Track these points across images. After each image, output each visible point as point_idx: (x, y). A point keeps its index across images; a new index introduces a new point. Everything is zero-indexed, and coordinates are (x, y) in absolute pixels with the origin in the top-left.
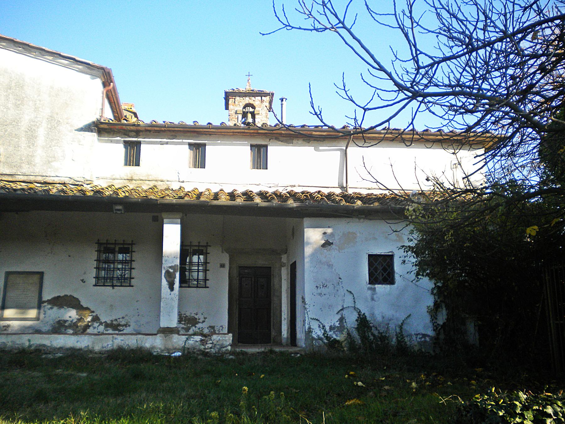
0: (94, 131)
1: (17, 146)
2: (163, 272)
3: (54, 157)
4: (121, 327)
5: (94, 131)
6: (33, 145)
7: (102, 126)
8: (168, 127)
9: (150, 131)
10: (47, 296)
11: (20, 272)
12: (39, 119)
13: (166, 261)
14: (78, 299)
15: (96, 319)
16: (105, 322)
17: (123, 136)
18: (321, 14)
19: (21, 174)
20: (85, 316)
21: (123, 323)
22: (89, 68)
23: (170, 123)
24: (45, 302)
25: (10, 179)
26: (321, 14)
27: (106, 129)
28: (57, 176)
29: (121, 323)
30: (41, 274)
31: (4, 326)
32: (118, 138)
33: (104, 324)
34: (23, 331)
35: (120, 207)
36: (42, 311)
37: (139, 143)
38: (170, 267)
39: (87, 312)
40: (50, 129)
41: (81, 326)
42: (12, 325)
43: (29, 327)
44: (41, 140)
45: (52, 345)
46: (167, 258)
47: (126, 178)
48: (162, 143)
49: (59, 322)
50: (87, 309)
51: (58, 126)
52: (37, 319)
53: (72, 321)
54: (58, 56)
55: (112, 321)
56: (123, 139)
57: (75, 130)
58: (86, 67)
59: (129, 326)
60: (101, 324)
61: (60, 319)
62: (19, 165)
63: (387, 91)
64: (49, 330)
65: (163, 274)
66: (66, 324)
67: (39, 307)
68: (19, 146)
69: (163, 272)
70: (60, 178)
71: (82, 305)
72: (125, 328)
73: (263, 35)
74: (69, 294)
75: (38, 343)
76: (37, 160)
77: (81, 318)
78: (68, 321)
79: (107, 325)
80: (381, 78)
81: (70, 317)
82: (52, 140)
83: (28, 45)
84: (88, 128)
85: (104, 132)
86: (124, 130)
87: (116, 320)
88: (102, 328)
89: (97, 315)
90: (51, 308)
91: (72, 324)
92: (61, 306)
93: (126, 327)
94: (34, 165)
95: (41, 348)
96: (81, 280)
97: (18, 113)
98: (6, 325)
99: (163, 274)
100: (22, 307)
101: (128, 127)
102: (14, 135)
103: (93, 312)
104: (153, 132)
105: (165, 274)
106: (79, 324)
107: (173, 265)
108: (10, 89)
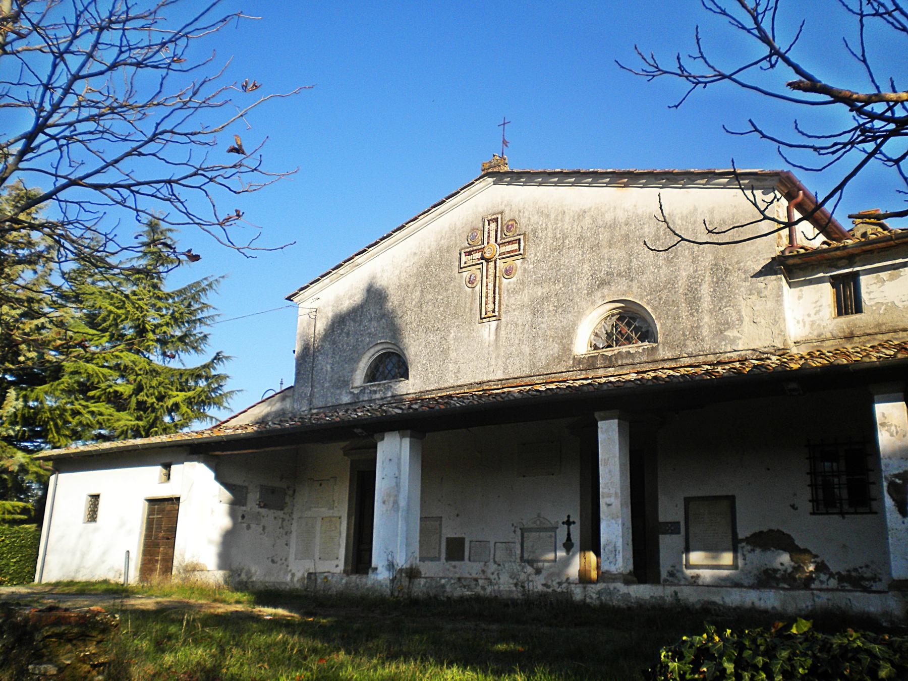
0: (779, 272)
1: (676, 317)
2: (885, 484)
3: (728, 323)
4: (867, 583)
5: (779, 272)
6: (697, 310)
7: (791, 261)
8: (897, 239)
9: (871, 251)
10: (743, 533)
11: (706, 497)
12: (700, 272)
13: (887, 466)
14: (789, 536)
15: (821, 567)
16: (838, 573)
17: (828, 270)
18: (695, 58)
19: (686, 355)
20: (805, 564)
21: (868, 574)
22: (757, 180)
23: (902, 230)
24: (742, 541)
25: (673, 365)
26: (695, 58)
27: (799, 265)
28: (735, 351)
29: (865, 576)
30: (731, 499)
31: (692, 577)
32: (821, 275)
33: (836, 577)
34: (719, 584)
35: (793, 385)
36: (739, 555)
37: (856, 275)
38: (897, 476)
39: (806, 557)
40: (717, 283)
41: (800, 578)
42: (702, 575)
43: (726, 579)
44: (706, 303)
45: (724, 602)
46: (887, 461)
47: (841, 335)
48: (895, 266)
49: (766, 572)
50: (806, 551)
51: (726, 277)
52: (735, 566)
53: (785, 571)
54: (712, 175)
55: (848, 571)
56: (828, 275)
57: (752, 277)
58: (755, 179)
59: (880, 580)
60: (831, 575)
61: (768, 567)
62: (682, 343)
63: (219, 241)
64: (753, 584)
65: (885, 489)
66: (778, 576)
67: (735, 550)
68: (679, 317)
69: (885, 484)
70: (739, 353)
71: (797, 546)
72: (874, 584)
73: (677, 107)
74: (775, 528)
75: (706, 599)
76: (705, 331)
77: (799, 566)
78: (779, 570)
79: (841, 578)
80: (742, 134)
81: (782, 564)
82: (721, 299)
83: (671, 173)
84: (768, 270)
85: (798, 271)
86: (828, 260)
87: (856, 570)
88: (833, 583)
89: (823, 561)
90: (753, 550)
91: (787, 576)
92: (765, 547)
93: (875, 582)
94: (703, 340)
95: (710, 606)
96: (791, 506)
97: (672, 271)
98: (695, 575)
99: (885, 489)
100: (713, 548)
101: (833, 253)
102: (671, 303)
103: (816, 556)
104: (879, 252)
105: (888, 487)
106: (797, 576)
107: (901, 471)
108: (659, 240)
